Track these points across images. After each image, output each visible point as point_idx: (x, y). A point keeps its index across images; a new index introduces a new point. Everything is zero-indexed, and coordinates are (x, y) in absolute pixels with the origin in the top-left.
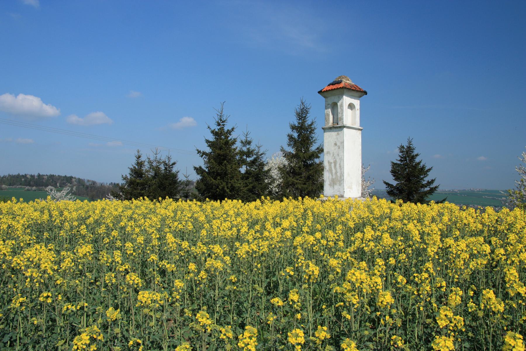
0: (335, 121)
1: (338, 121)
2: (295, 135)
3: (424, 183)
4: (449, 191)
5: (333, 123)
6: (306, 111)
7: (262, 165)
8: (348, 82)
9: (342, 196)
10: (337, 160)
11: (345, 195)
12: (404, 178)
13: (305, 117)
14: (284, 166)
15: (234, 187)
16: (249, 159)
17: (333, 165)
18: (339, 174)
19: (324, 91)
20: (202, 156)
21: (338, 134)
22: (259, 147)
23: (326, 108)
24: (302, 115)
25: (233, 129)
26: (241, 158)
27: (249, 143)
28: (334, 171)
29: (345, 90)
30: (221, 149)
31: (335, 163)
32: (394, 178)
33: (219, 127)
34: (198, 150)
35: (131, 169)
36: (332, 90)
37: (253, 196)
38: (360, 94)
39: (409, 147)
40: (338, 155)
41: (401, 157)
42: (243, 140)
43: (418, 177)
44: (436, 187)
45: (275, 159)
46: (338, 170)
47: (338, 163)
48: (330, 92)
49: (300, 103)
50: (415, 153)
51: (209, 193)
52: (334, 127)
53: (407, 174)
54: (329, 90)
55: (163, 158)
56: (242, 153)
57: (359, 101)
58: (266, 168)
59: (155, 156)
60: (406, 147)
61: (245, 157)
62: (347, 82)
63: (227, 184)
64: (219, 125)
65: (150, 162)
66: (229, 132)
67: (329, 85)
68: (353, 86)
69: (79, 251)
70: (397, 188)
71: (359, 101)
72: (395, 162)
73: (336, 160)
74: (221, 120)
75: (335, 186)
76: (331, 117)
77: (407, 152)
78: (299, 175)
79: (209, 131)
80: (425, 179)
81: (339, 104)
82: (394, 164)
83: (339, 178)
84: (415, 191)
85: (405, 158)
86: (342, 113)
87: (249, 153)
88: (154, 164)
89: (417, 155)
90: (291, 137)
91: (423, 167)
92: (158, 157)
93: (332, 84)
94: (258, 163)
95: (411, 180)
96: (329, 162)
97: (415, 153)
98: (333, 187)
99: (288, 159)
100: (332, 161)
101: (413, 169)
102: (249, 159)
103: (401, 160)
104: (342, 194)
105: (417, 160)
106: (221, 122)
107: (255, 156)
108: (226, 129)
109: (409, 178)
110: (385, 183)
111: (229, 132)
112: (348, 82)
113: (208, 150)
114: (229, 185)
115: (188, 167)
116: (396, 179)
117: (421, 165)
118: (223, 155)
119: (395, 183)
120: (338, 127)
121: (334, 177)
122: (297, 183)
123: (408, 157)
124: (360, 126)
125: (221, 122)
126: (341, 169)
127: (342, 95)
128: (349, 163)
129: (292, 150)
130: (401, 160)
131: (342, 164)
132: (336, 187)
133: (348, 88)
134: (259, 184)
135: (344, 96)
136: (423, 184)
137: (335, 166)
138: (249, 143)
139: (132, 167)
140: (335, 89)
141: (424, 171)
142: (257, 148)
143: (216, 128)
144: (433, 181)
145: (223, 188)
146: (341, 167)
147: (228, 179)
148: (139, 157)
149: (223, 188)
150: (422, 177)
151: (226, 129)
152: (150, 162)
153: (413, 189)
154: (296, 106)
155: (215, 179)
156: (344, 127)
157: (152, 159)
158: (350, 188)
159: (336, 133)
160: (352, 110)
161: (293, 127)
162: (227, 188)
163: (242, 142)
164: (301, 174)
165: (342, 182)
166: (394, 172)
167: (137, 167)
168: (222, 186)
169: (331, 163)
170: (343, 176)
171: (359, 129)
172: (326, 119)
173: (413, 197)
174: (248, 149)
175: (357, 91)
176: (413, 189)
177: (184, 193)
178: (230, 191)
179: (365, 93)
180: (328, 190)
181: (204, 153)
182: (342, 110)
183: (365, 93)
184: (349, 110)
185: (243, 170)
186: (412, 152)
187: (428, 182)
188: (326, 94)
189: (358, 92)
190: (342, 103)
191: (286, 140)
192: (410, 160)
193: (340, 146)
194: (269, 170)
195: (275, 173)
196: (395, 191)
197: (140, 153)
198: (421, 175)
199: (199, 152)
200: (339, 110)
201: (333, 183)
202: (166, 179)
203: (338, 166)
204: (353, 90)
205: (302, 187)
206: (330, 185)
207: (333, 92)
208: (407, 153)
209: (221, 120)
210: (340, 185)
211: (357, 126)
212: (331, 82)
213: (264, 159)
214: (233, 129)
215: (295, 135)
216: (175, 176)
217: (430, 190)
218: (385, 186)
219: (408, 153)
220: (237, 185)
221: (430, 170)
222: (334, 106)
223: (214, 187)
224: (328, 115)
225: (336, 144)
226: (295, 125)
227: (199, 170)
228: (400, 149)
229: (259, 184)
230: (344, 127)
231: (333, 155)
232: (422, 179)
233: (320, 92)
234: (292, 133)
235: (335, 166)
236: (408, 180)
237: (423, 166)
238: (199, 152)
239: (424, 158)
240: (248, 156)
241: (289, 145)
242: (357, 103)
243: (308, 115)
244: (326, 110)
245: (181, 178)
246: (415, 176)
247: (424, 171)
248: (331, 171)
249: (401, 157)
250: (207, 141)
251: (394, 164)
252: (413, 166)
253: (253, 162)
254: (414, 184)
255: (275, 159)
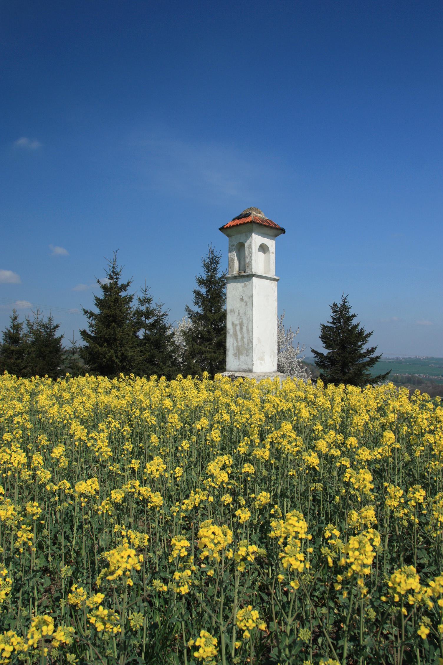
0: (241, 268)
1: (245, 268)
2: (203, 291)
3: (363, 351)
4: (393, 359)
5: (239, 270)
6: (216, 261)
7: (164, 328)
8: (259, 215)
9: (250, 371)
10: (244, 321)
11: (254, 370)
12: (337, 345)
13: (215, 268)
14: (190, 330)
15: (126, 357)
16: (148, 322)
17: (238, 327)
18: (246, 340)
19: (227, 227)
20: (89, 318)
21: (245, 285)
22: (160, 306)
23: (230, 251)
24: (211, 265)
25: (128, 284)
26: (138, 319)
27: (149, 301)
28: (239, 337)
29: (255, 226)
30: (109, 307)
31: (241, 325)
32: (324, 345)
33: (111, 281)
34: (84, 310)
35: (5, 334)
36: (237, 225)
37: (152, 367)
38: (275, 231)
39: (343, 306)
40: (245, 314)
41: (334, 319)
42: (141, 298)
43: (355, 344)
44: (377, 357)
45: (179, 323)
46: (246, 335)
47: (246, 325)
48: (235, 228)
49: (208, 251)
50: (351, 313)
51: (95, 364)
52: (239, 276)
53: (341, 340)
54: (233, 226)
55: (45, 321)
56: (138, 313)
57: (274, 242)
58: (169, 332)
59: (36, 317)
60: (339, 306)
61: (143, 319)
62: (257, 215)
63: (116, 352)
64: (111, 278)
65: (30, 325)
66: (124, 287)
67: (234, 220)
68: (266, 221)
69: (158, 391)
70: (327, 358)
71: (274, 242)
72: (326, 324)
73: (242, 322)
74: (114, 272)
75: (241, 357)
76: (236, 262)
77: (341, 312)
78: (208, 341)
79: (98, 286)
80: (363, 346)
81: (246, 245)
82: (324, 328)
83: (246, 345)
84: (351, 362)
85: (339, 319)
86: (251, 257)
87: (148, 314)
88: (35, 327)
89: (353, 316)
90: (198, 294)
91: (362, 332)
92: (40, 318)
93: (238, 218)
94: (158, 327)
95: (346, 348)
96: (233, 324)
97: (351, 313)
98: (239, 359)
99: (194, 322)
100: (237, 322)
101: (348, 334)
102: (148, 322)
103: (333, 323)
104: (250, 367)
105: (354, 322)
106: (114, 275)
107: (155, 318)
108: (120, 283)
109: (343, 345)
110: (313, 351)
111: (124, 287)
112: (259, 215)
113: (97, 311)
114: (119, 354)
115: (72, 333)
116: (327, 347)
117: (359, 328)
118: (113, 316)
119: (325, 352)
120: (245, 276)
121: (240, 344)
122: (205, 352)
123: (342, 318)
124: (276, 275)
125: (114, 275)
126: (249, 334)
127: (251, 232)
128: (262, 327)
129: (198, 309)
130: (333, 323)
131: (250, 327)
132: (243, 358)
133: (258, 223)
134: (160, 352)
135: (253, 235)
136: (361, 354)
137: (241, 328)
138: (149, 301)
139: (7, 331)
140: (240, 224)
141: (362, 337)
142: (157, 307)
143: (106, 281)
144: (373, 350)
145: (111, 357)
146: (249, 331)
147: (117, 347)
148: (15, 318)
149: (111, 357)
150: (360, 344)
151: (120, 283)
152: (30, 325)
153: (349, 359)
154: (204, 255)
155: (101, 346)
156: (253, 275)
157: (32, 320)
158: (262, 359)
159: (242, 284)
160: (264, 253)
161: (200, 281)
162: (117, 357)
163: (140, 300)
164: (211, 340)
165: (250, 351)
166: (325, 338)
167: (12, 331)
168: (109, 355)
169: (236, 325)
170: (252, 342)
171: (274, 280)
172: (231, 265)
173: (349, 369)
174: (147, 308)
175: (272, 228)
176: (349, 359)
177: (70, 364)
178: (121, 362)
179: (283, 231)
180: (232, 362)
181: (92, 314)
182: (251, 253)
183: (283, 231)
184: (261, 254)
185: (141, 334)
186: (348, 312)
187: (368, 350)
188: (229, 231)
189: (274, 230)
190: (251, 243)
191: (192, 297)
192: (345, 323)
193: (247, 301)
194: (173, 334)
195: (179, 340)
196: (326, 362)
197: (17, 313)
198: (358, 341)
199: (86, 312)
200: (247, 253)
201: (239, 352)
202: (46, 346)
203: (245, 328)
204: (265, 226)
205: (211, 357)
206: (235, 355)
207: (239, 228)
208: (341, 313)
209: (114, 272)
210: (247, 356)
211: (272, 274)
212: (237, 215)
213: (166, 321)
214: (128, 284)
215: (203, 291)
216: (58, 341)
217: (370, 361)
218: (313, 355)
219: (342, 314)
220: (130, 353)
221: (370, 334)
222: (240, 248)
223: (101, 356)
224: (233, 260)
225: (242, 299)
226: (202, 278)
227: (84, 333)
228: (333, 308)
229: (160, 352)
230: (253, 275)
231: (239, 314)
232: (360, 346)
233: (222, 229)
234: (199, 289)
235: (241, 328)
236: (343, 348)
237: (362, 329)
238: (86, 312)
239: (363, 318)
240: (148, 318)
241: (196, 304)
242: (271, 243)
243: (219, 266)
244: (230, 254)
245: (66, 344)
246: (351, 343)
247: (362, 337)
248: (235, 335)
249: (334, 319)
250: (97, 299)
251: (324, 328)
252: (349, 330)
253: (153, 325)
254: (350, 353)
255: (179, 323)
